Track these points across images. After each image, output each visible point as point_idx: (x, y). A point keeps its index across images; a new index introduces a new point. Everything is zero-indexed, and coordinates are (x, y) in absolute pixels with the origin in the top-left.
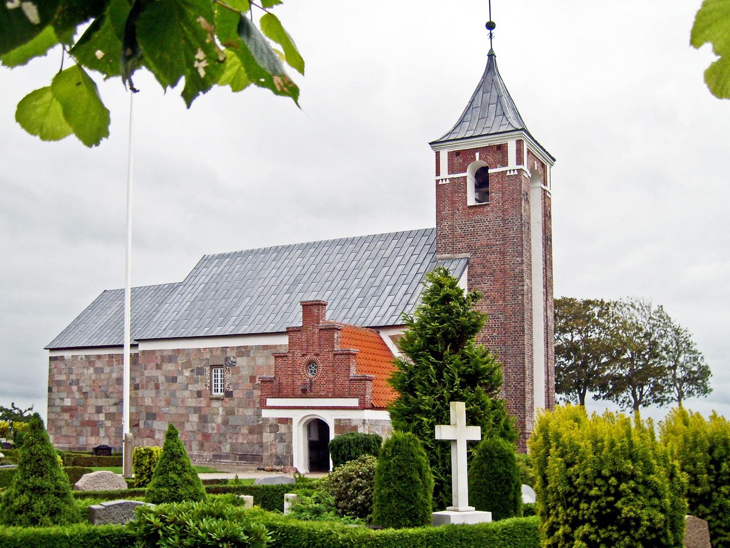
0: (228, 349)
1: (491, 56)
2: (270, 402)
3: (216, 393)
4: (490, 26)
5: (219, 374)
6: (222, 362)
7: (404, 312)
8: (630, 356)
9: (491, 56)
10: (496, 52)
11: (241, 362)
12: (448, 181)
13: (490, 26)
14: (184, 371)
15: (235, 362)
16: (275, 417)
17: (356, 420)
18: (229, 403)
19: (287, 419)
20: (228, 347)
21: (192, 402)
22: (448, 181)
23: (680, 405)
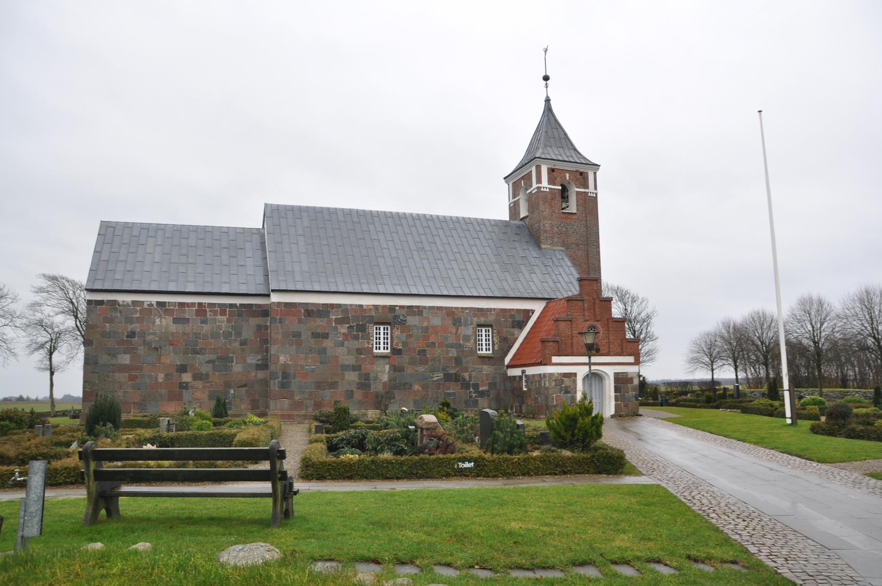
0: (397, 308)
1: (548, 100)
2: (555, 359)
3: (378, 351)
4: (546, 78)
5: (382, 331)
6: (391, 321)
7: (429, 276)
8: (82, 340)
9: (548, 100)
10: (551, 98)
11: (412, 320)
12: (548, 190)
13: (546, 78)
14: (339, 326)
15: (405, 321)
16: (560, 372)
17: (632, 373)
18: (397, 360)
19: (571, 374)
20: (397, 306)
21: (350, 360)
22: (548, 190)
23: (737, 376)
